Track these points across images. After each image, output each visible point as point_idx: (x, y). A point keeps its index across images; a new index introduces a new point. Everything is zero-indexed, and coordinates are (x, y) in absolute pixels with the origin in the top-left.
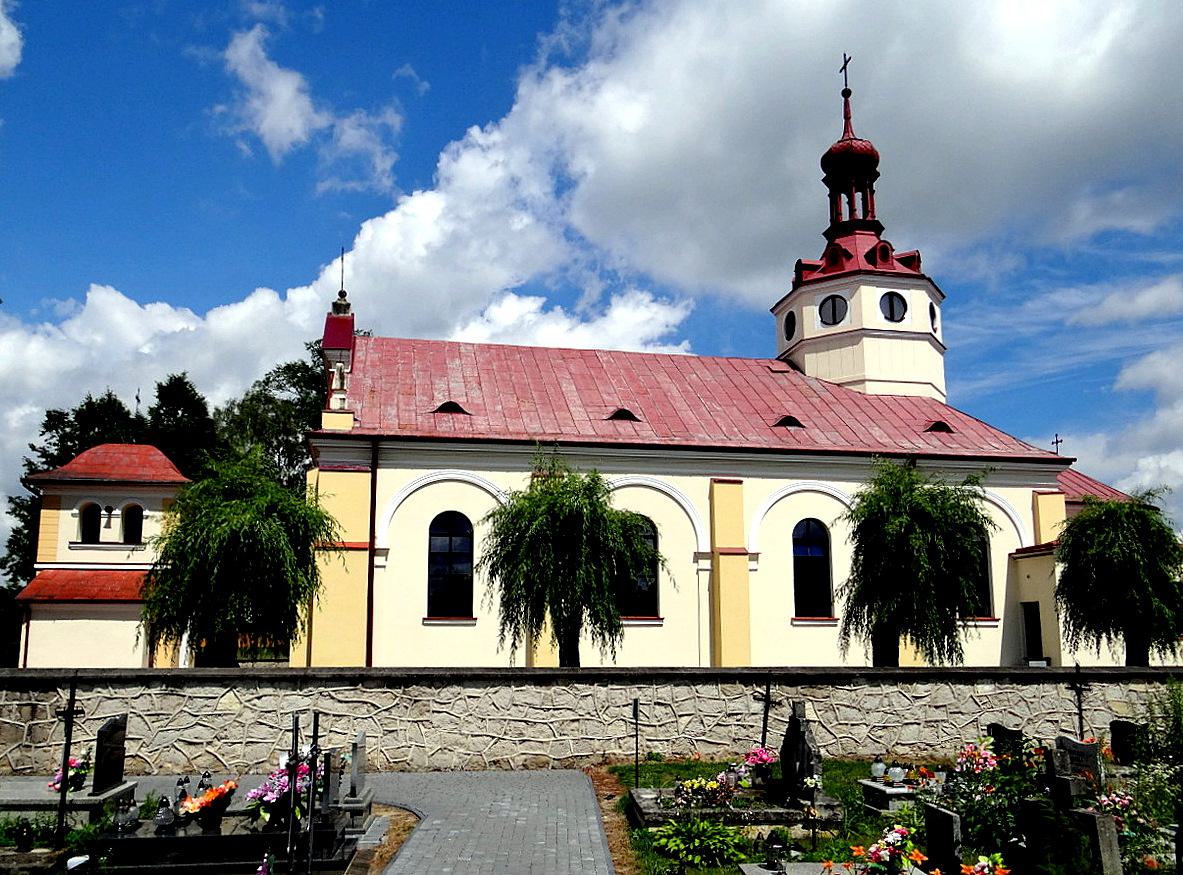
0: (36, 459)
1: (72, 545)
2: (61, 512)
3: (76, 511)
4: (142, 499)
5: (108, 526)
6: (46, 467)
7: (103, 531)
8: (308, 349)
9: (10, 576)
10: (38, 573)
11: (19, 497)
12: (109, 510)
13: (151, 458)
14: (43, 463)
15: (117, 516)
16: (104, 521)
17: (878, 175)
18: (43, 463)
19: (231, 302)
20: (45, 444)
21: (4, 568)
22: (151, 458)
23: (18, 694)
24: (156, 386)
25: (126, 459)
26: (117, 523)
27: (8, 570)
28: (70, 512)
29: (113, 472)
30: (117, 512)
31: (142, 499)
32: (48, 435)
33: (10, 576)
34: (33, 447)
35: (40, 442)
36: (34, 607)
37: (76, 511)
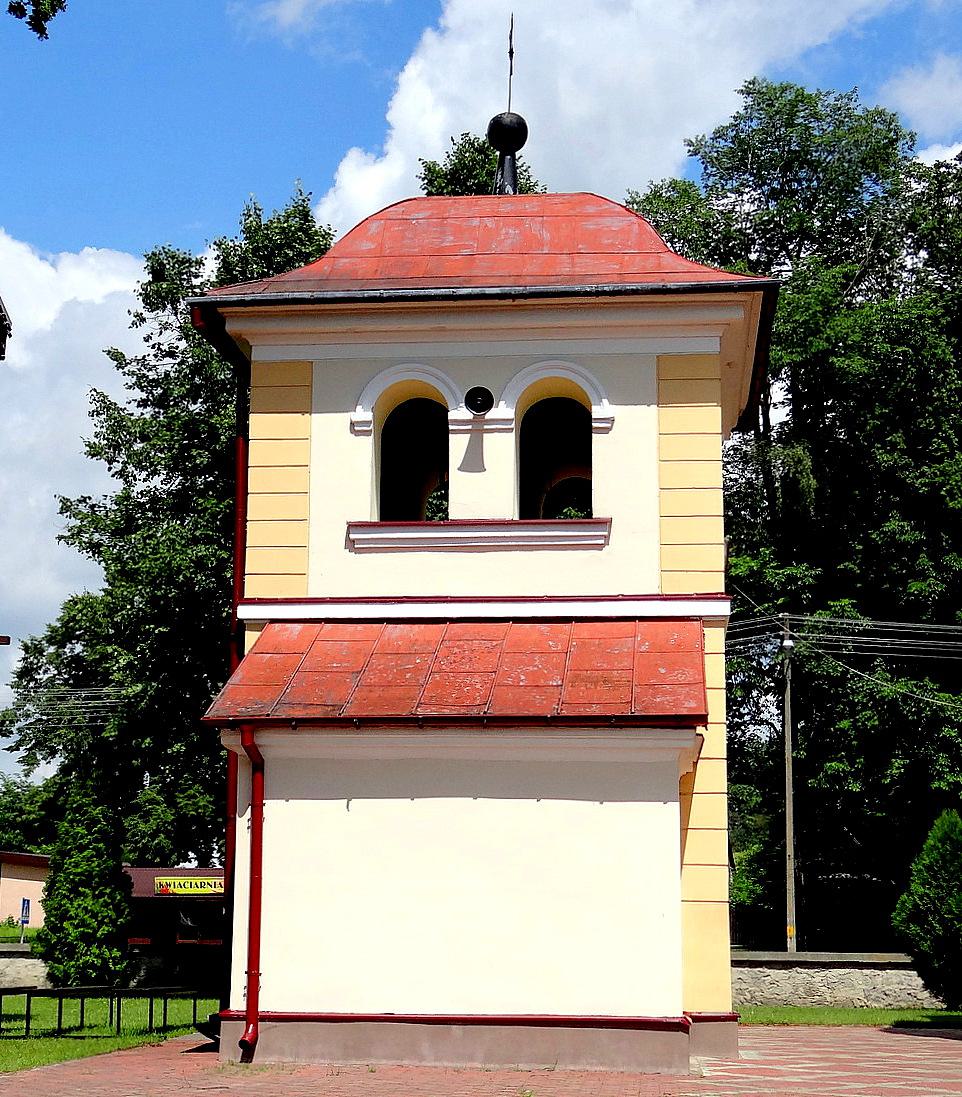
0: (126, 397)
1: (357, 537)
2: (317, 419)
3: (363, 414)
4: (579, 359)
5: (474, 462)
6: (148, 412)
7: (457, 479)
8: (695, 153)
9: (22, 752)
10: (251, 638)
11: (84, 500)
12: (480, 400)
13: (591, 225)
14: (143, 403)
15: (501, 426)
16: (458, 445)
17: (602, 803)
18: (143, 403)
19: (319, 199)
20: (144, 350)
21: (7, 734)
22: (591, 225)
23: (904, 897)
24: (422, 170)
25: (510, 236)
26: (502, 451)
27: (16, 737)
28: (342, 420)
29: (475, 272)
30: (503, 411)
31: (579, 359)
32: (151, 326)
33: (22, 752)
34: (118, 358)
35: (135, 347)
36: (273, 744)
37: (363, 414)
